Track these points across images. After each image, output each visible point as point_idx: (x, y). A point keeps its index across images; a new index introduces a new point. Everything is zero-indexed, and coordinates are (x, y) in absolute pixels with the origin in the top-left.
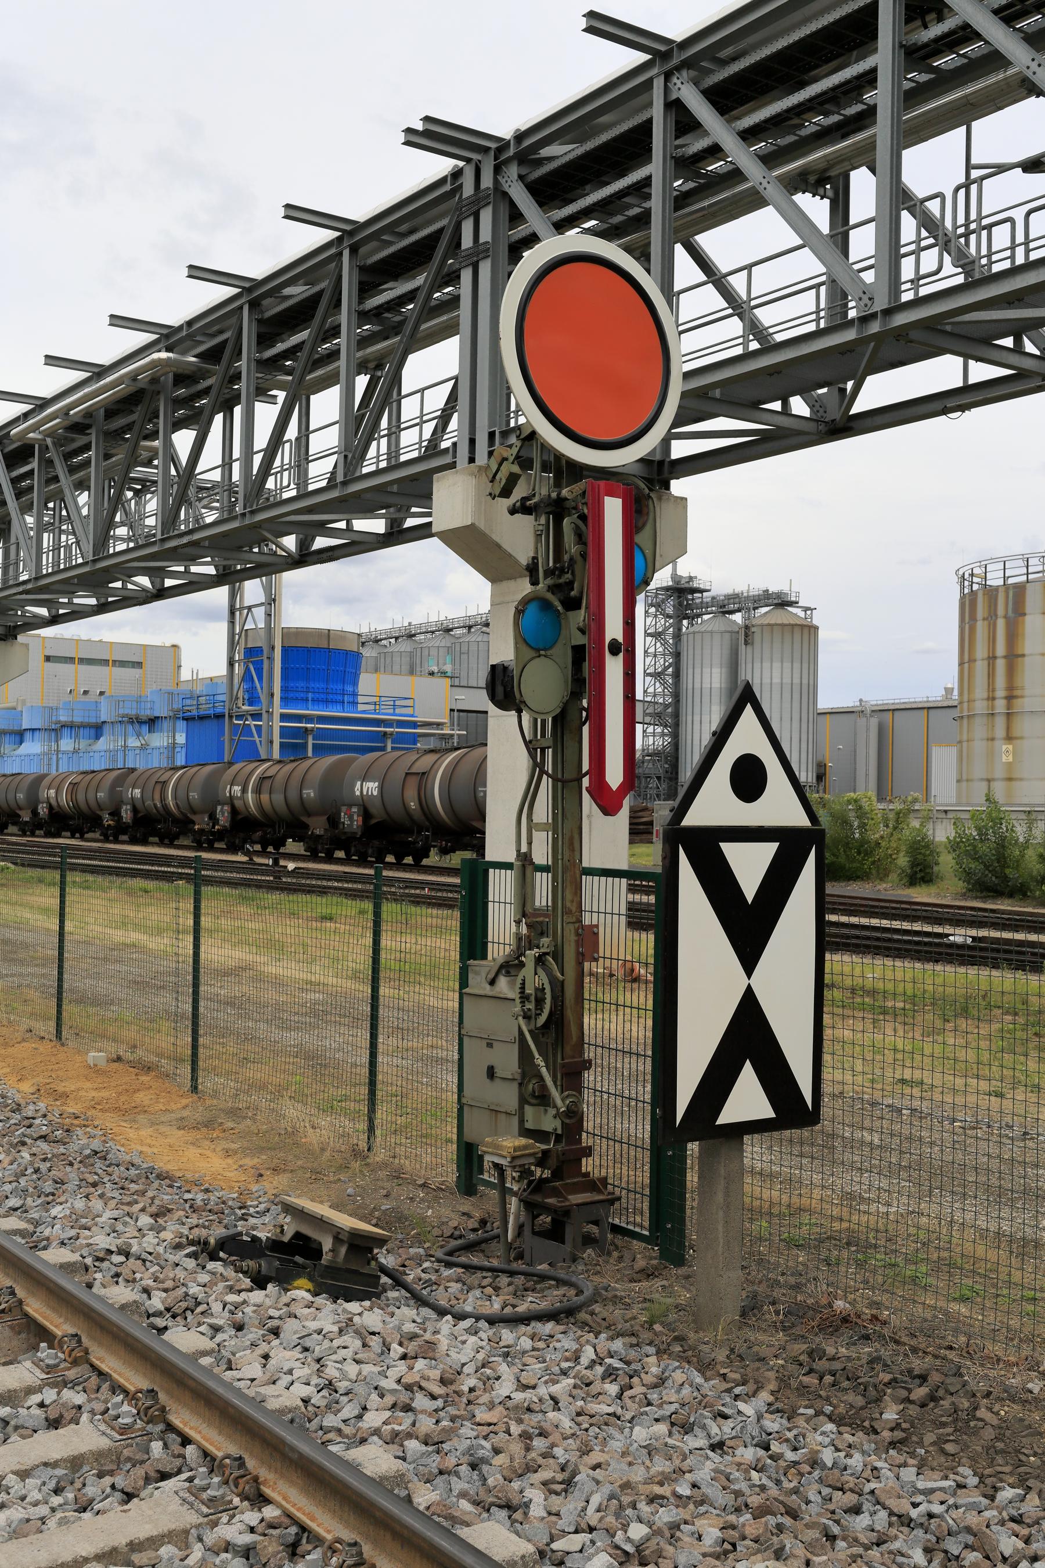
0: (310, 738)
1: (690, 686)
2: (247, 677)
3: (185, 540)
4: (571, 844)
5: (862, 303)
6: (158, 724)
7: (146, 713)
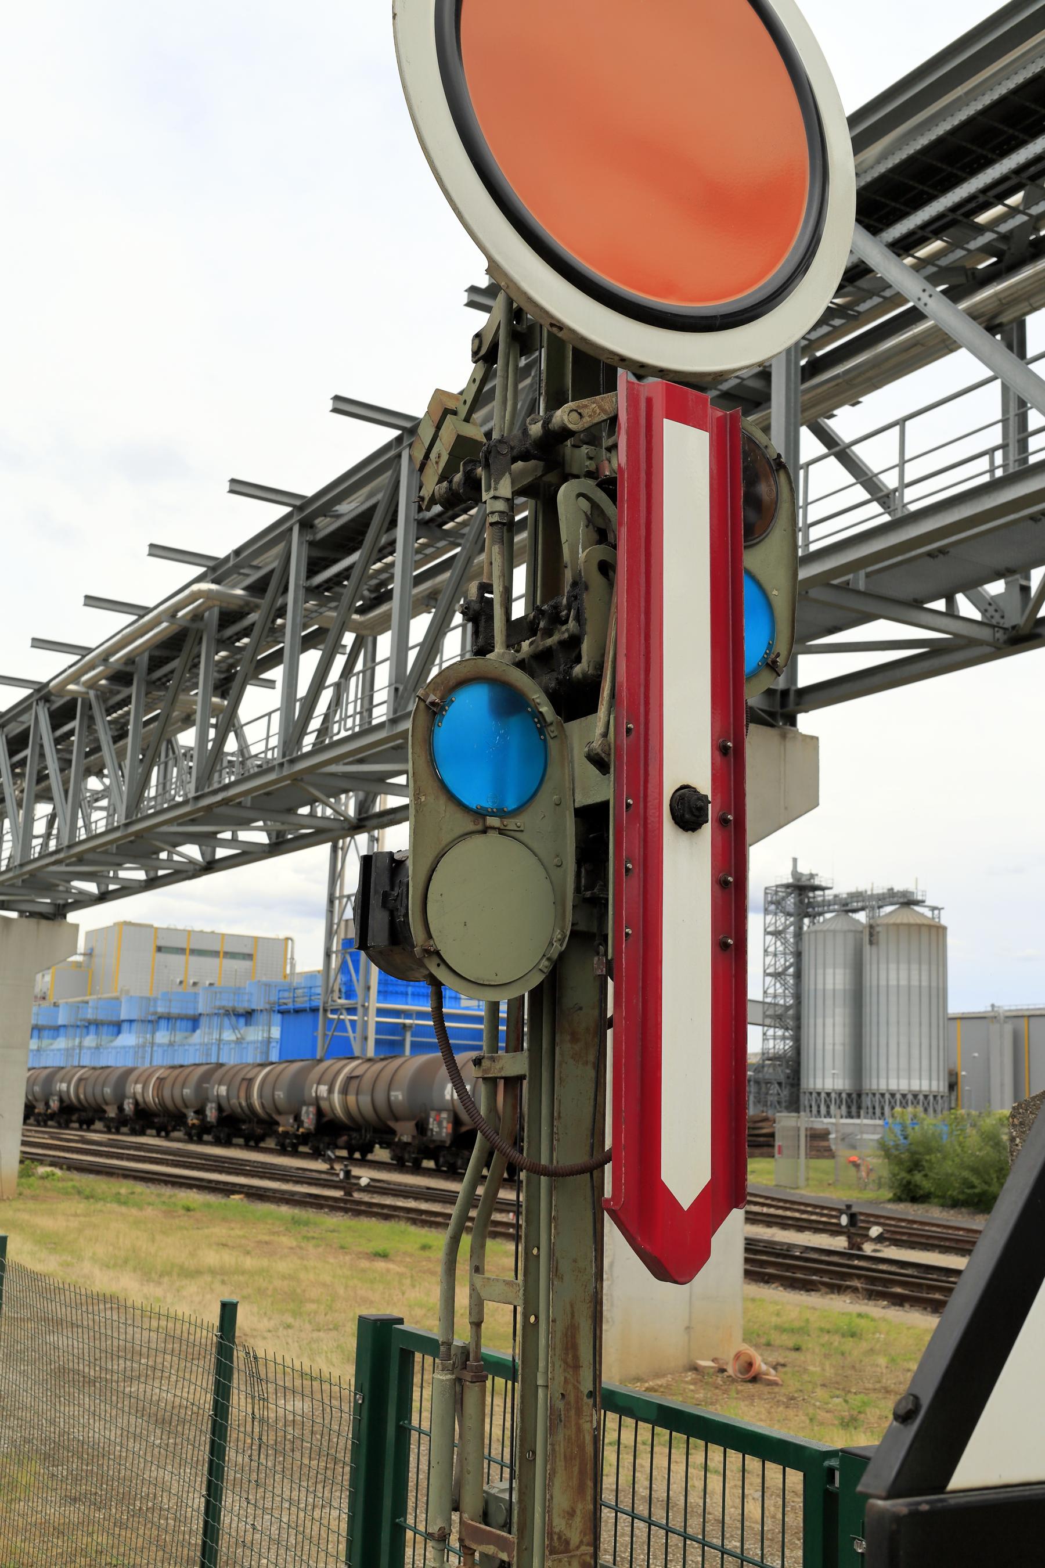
1: (812, 987)
2: (343, 968)
4: (571, 1345)
6: (256, 1015)
7: (243, 1005)
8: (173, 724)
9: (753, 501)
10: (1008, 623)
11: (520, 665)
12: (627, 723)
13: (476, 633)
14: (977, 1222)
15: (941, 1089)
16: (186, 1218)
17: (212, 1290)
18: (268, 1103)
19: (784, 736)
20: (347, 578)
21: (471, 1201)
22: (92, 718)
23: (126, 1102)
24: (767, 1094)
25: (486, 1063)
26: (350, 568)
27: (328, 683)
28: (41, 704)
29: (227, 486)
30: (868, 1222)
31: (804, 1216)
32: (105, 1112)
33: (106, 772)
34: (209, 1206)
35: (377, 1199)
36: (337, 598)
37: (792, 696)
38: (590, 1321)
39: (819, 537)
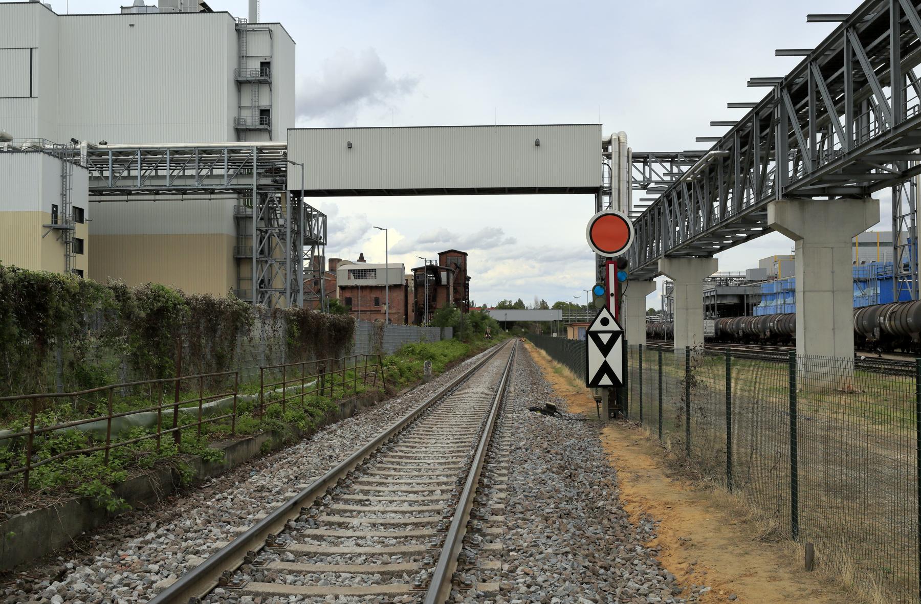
18: (861, 327)
28: (851, 30)
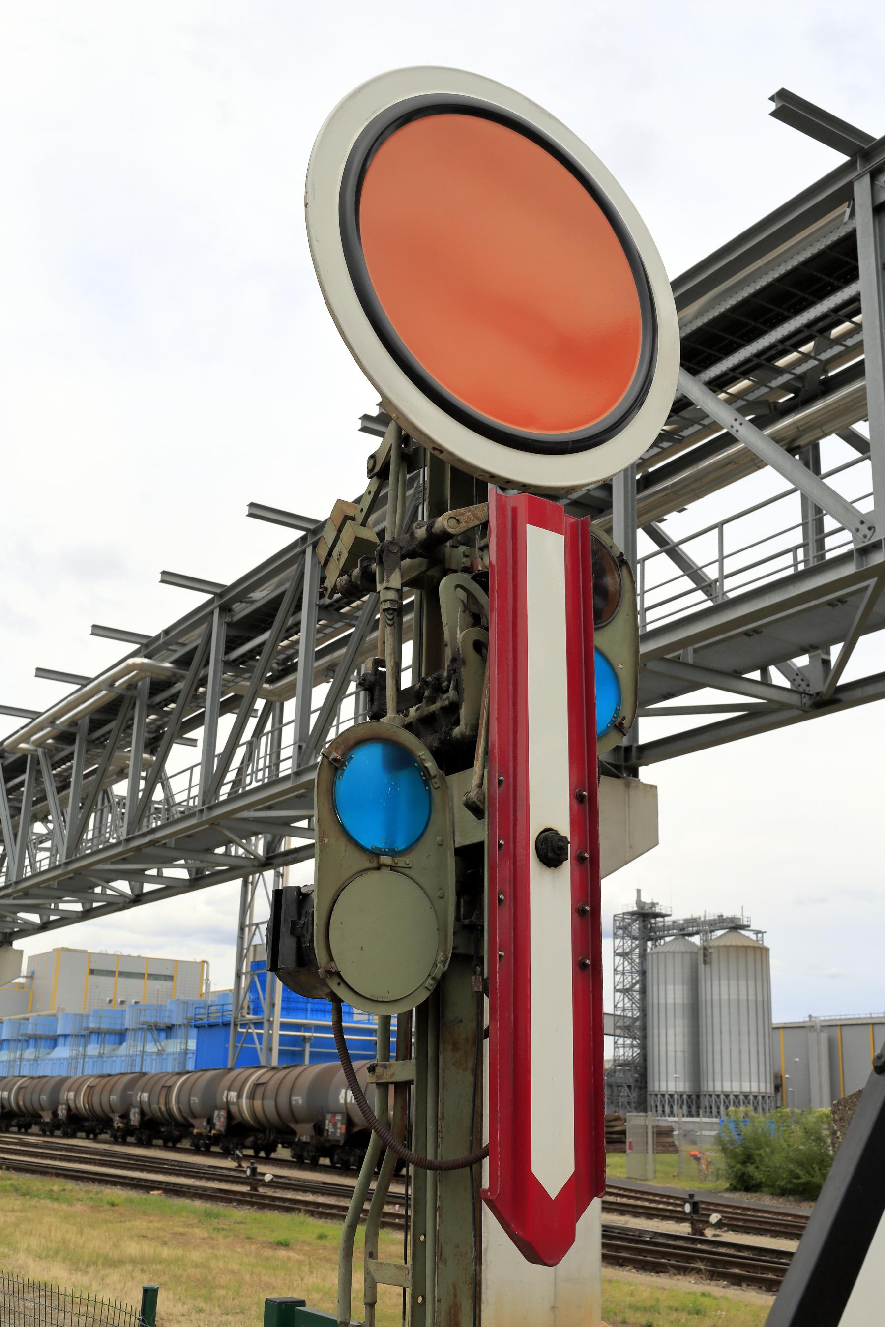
0: (308, 1046)
1: (656, 1001)
2: (252, 987)
3: (147, 839)
5: (860, 535)
7: (165, 1021)
8: (109, 777)
9: (601, 591)
10: (813, 691)
11: (409, 727)
12: (499, 776)
13: (372, 701)
14: (804, 1209)
15: (768, 1090)
16: (111, 1213)
17: (133, 1278)
19: (628, 785)
20: (259, 654)
21: (366, 1194)
22: (39, 772)
23: (60, 1108)
24: (618, 1096)
25: (379, 1070)
26: (262, 644)
27: (242, 742)
29: (159, 577)
30: (709, 1210)
31: (653, 1205)
32: (41, 1117)
33: (50, 818)
34: (131, 1201)
35: (279, 1194)
36: (250, 670)
37: (634, 751)
38: (470, 1301)
39: (654, 619)
